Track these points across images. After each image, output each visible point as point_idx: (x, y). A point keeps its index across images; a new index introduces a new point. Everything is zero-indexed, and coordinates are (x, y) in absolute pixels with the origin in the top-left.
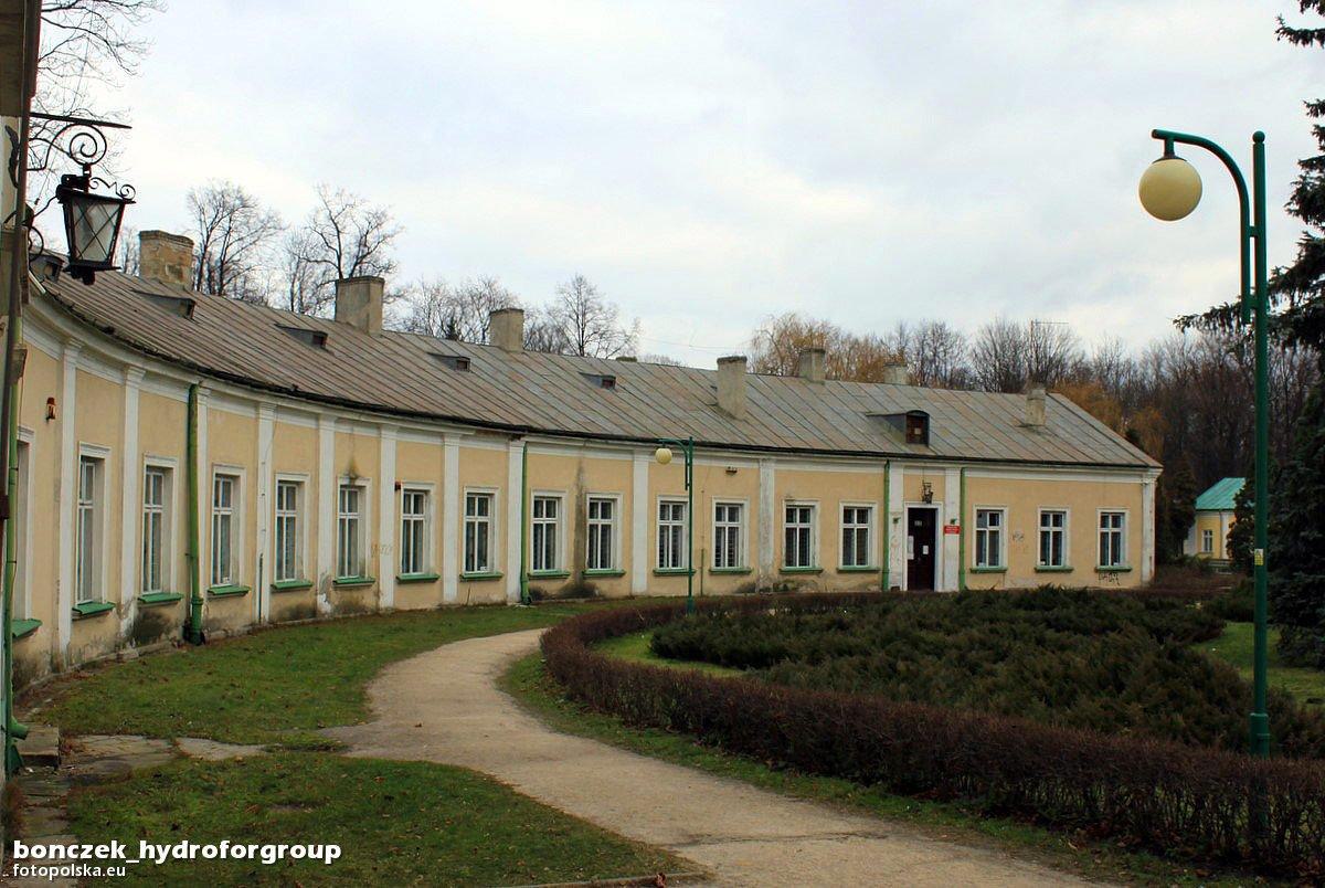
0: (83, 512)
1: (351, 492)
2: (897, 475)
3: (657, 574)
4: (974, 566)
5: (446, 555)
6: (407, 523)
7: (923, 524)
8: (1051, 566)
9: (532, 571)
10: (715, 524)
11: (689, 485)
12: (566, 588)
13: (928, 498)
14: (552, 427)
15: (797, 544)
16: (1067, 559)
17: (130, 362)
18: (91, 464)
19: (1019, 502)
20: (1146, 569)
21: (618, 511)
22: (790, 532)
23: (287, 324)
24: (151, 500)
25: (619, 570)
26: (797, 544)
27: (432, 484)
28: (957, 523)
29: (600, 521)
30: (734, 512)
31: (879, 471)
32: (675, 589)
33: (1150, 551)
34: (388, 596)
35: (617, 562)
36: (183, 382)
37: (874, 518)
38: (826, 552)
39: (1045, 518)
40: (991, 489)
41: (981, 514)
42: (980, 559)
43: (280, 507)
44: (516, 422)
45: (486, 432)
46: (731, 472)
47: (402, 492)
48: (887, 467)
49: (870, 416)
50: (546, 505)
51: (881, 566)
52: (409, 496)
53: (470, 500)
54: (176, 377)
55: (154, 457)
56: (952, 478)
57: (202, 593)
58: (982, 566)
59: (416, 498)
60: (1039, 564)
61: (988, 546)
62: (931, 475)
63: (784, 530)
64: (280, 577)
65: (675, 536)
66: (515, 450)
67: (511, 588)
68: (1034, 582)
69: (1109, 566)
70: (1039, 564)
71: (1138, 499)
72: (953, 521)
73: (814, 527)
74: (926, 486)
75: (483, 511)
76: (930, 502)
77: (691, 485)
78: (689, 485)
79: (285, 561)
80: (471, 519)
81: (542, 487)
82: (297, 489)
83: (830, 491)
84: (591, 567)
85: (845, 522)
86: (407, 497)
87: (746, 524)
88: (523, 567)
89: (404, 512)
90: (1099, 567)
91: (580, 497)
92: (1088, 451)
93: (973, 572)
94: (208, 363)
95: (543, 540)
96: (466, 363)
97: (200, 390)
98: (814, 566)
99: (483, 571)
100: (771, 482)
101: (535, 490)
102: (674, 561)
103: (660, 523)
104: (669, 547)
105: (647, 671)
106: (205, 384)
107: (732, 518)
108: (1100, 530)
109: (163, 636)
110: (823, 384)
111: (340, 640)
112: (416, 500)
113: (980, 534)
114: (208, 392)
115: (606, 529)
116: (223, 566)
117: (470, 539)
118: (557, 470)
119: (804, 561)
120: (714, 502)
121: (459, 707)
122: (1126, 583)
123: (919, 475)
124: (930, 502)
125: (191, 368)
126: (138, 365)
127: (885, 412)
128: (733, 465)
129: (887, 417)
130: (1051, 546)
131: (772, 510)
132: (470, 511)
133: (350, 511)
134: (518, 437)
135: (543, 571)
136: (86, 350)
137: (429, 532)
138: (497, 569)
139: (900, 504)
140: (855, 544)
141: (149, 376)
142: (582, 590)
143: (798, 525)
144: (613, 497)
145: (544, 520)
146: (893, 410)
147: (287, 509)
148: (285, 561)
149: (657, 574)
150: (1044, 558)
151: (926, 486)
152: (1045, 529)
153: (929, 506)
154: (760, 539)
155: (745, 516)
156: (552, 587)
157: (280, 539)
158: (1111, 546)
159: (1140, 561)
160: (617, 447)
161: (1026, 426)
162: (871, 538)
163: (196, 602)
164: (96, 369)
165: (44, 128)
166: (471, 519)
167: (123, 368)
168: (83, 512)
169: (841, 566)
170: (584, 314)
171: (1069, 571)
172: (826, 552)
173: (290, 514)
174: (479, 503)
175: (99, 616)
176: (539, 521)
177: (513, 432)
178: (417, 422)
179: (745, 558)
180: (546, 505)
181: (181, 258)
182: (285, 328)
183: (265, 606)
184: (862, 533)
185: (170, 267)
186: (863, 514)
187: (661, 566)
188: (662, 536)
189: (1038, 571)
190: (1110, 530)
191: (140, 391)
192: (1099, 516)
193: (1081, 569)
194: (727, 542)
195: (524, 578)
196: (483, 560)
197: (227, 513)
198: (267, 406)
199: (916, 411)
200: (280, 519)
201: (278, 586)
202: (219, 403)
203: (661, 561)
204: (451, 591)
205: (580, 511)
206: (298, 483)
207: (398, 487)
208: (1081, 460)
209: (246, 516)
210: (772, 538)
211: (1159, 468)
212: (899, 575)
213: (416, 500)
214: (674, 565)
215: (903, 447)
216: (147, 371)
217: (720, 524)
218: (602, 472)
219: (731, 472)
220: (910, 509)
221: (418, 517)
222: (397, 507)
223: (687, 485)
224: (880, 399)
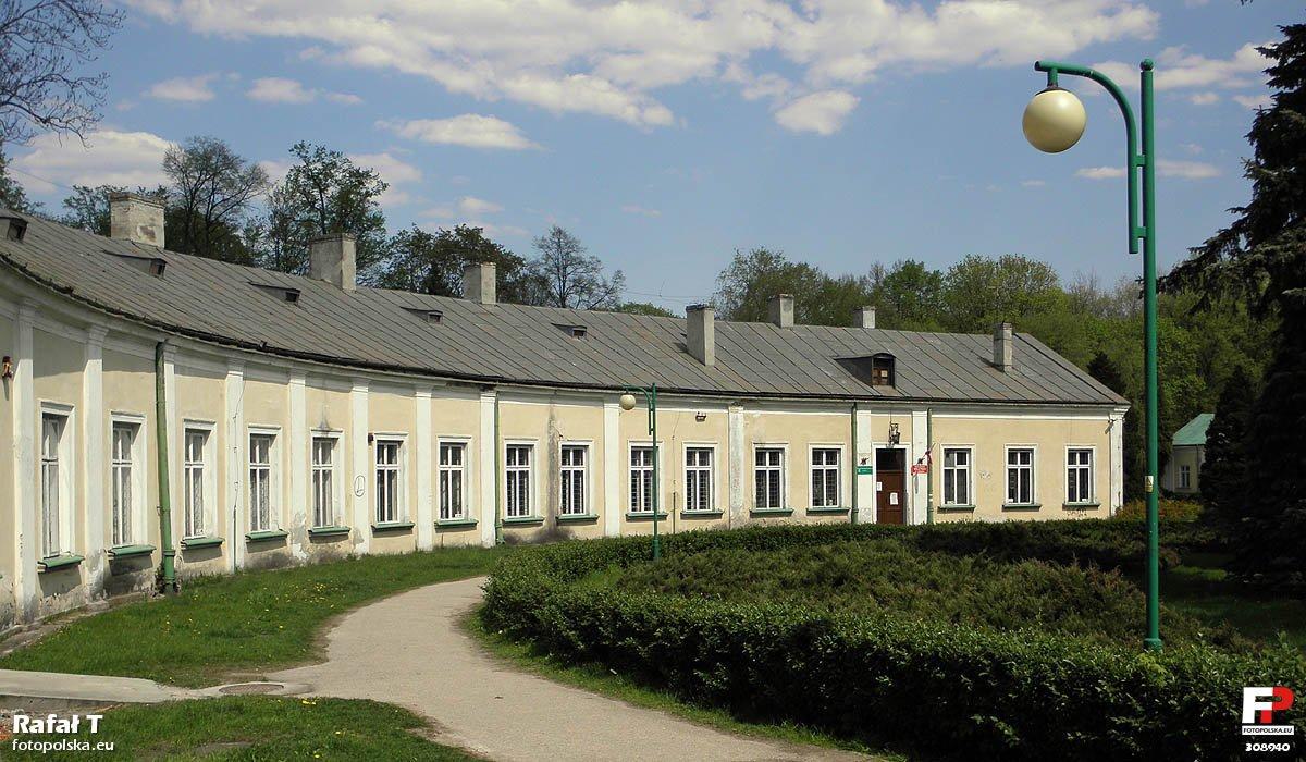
0: (191, 472)
1: (324, 444)
2: (864, 416)
3: (630, 519)
4: (943, 505)
5: (420, 506)
6: (381, 473)
7: (890, 463)
8: (1019, 503)
9: (507, 518)
11: (652, 430)
12: (540, 532)
13: (895, 439)
14: (524, 377)
15: (769, 486)
16: (1037, 496)
17: (91, 321)
18: (55, 421)
19: (988, 438)
20: (1117, 501)
21: (590, 458)
22: (760, 475)
23: (262, 282)
25: (592, 515)
26: (769, 486)
27: (279, 429)
28: (925, 463)
29: (572, 468)
30: (705, 454)
32: (644, 529)
33: (1119, 487)
34: (365, 544)
35: (591, 507)
36: (151, 340)
38: (797, 499)
40: (957, 428)
41: (948, 452)
42: (949, 497)
44: (487, 373)
45: (458, 384)
46: (700, 418)
47: (375, 443)
50: (519, 453)
54: (141, 335)
55: (121, 414)
56: (920, 417)
57: (176, 545)
58: (950, 504)
60: (1009, 502)
61: (957, 484)
62: (899, 418)
64: (254, 528)
65: (576, 482)
66: (487, 401)
67: (486, 535)
68: (998, 517)
69: (1078, 502)
70: (1009, 502)
71: (1104, 435)
72: (920, 461)
74: (894, 427)
75: (456, 459)
76: (897, 443)
77: (654, 430)
78: (652, 430)
79: (260, 512)
80: (445, 467)
81: (513, 436)
83: (800, 433)
84: (564, 512)
86: (380, 448)
88: (497, 513)
91: (552, 446)
92: (1054, 389)
93: (941, 510)
94: (174, 320)
95: (518, 485)
96: (439, 316)
97: (167, 347)
98: (466, 518)
100: (740, 426)
102: (522, 509)
104: (644, 487)
106: (170, 342)
107: (576, 462)
108: (1068, 467)
109: (136, 587)
110: (159, 266)
111: (303, 593)
112: (388, 449)
113: (948, 473)
114: (175, 349)
115: (578, 474)
116: (194, 517)
117: (444, 491)
118: (529, 419)
119: (775, 503)
120: (1007, 449)
121: (403, 654)
122: (1101, 514)
123: (885, 419)
124: (897, 443)
125: (154, 325)
126: (99, 323)
127: (853, 356)
128: (702, 411)
130: (1020, 485)
131: (742, 454)
132: (444, 459)
133: (389, 462)
134: (490, 388)
135: (954, 504)
136: (41, 310)
137: (402, 481)
138: (472, 517)
139: (868, 449)
140: (825, 484)
141: (112, 334)
142: (557, 531)
143: (697, 468)
145: (517, 468)
146: (861, 353)
148: (260, 512)
150: (1012, 494)
151: (894, 427)
153: (896, 447)
154: (732, 483)
155: (716, 459)
156: (527, 533)
157: (254, 492)
158: (1080, 484)
159: (1108, 496)
160: (403, 381)
161: (580, 333)
163: (168, 554)
164: (56, 328)
165: (14, 95)
166: (445, 467)
167: (85, 327)
168: (191, 472)
169: (811, 507)
170: (565, 268)
171: (594, 520)
172: (797, 499)
174: (452, 451)
175: (69, 568)
176: (566, 468)
177: (482, 384)
179: (719, 499)
180: (519, 453)
181: (152, 219)
182: (258, 286)
183: (235, 556)
185: (142, 228)
186: (832, 455)
188: (634, 481)
189: (1005, 509)
190: (1078, 466)
191: (104, 349)
192: (505, 448)
193: (1050, 503)
194: (699, 485)
195: (500, 524)
196: (457, 508)
198: (237, 363)
199: (883, 354)
200: (253, 472)
201: (252, 537)
202: (187, 360)
203: (689, 504)
204: (426, 538)
205: (552, 456)
207: (370, 439)
208: (1048, 399)
210: (742, 480)
211: (1125, 404)
212: (868, 512)
213: (388, 449)
214: (575, 512)
216: (110, 329)
217: (691, 468)
218: (573, 421)
219: (700, 418)
220: (879, 452)
222: (370, 457)
223: (650, 430)
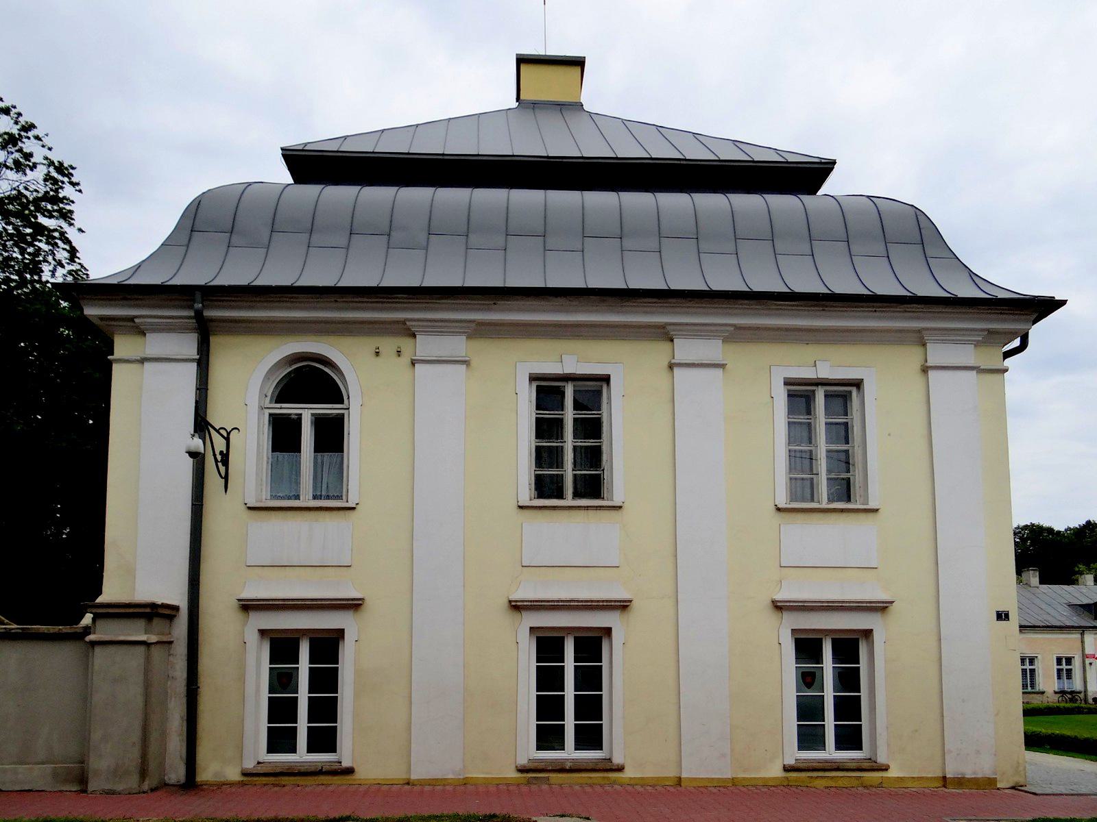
31: (1077, 636)
37: (1077, 663)
39: (1059, 661)
48: (1082, 634)
49: (1070, 605)
51: (1083, 690)
63: (1056, 670)
73: (1038, 668)
82: (566, 387)
85: (1058, 665)
87: (1040, 667)
127: (1081, 603)
129: (1080, 605)
143: (1028, 667)
146: (1085, 601)
162: (1075, 674)
178: (799, 391)
186: (1069, 661)
209: (489, 300)
215: (1093, 622)
224: (1076, 595)
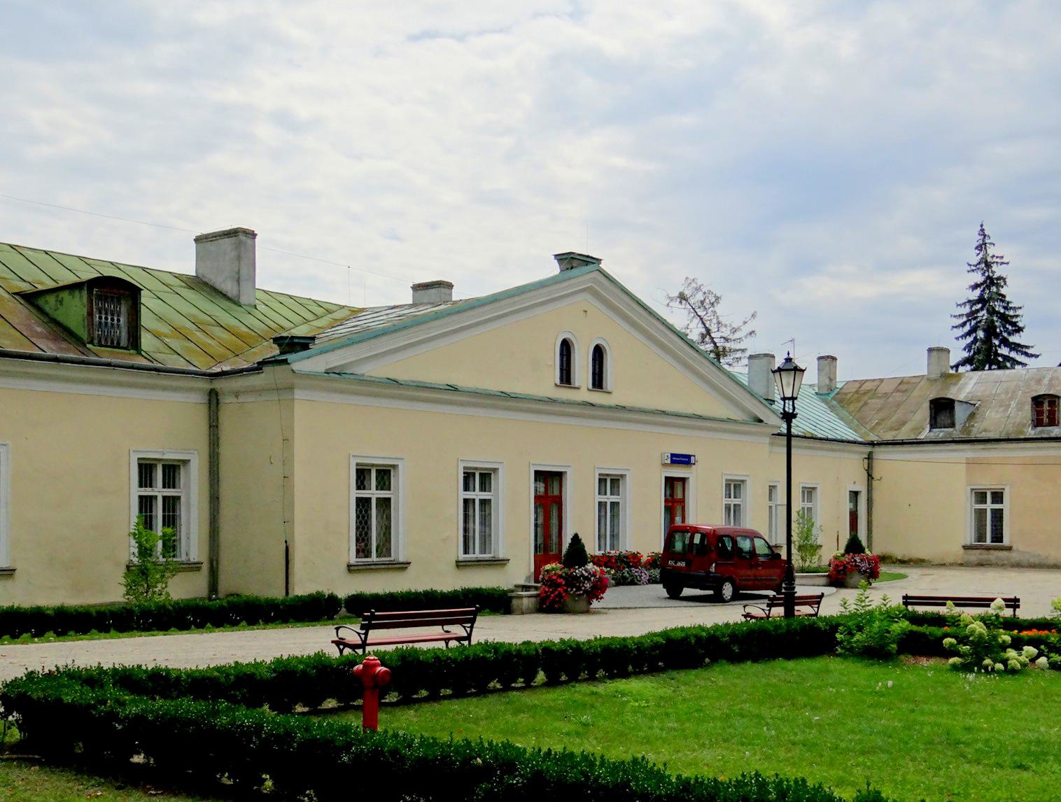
10: (355, 494)
24: (806, 501)
39: (362, 475)
43: (803, 501)
52: (730, 485)
53: (728, 486)
59: (735, 486)
75: (485, 485)
89: (599, 494)
90: (462, 557)
99: (487, 556)
101: (802, 483)
103: (726, 501)
105: (911, 632)
132: (602, 491)
144: (775, 484)
147: (611, 494)
149: (460, 565)
152: (364, 494)
173: (809, 505)
184: (171, 504)
186: (172, 472)
187: (466, 551)
197: (810, 506)
206: (743, 481)
221: (737, 501)
